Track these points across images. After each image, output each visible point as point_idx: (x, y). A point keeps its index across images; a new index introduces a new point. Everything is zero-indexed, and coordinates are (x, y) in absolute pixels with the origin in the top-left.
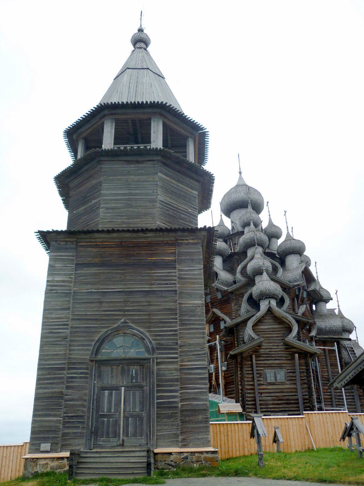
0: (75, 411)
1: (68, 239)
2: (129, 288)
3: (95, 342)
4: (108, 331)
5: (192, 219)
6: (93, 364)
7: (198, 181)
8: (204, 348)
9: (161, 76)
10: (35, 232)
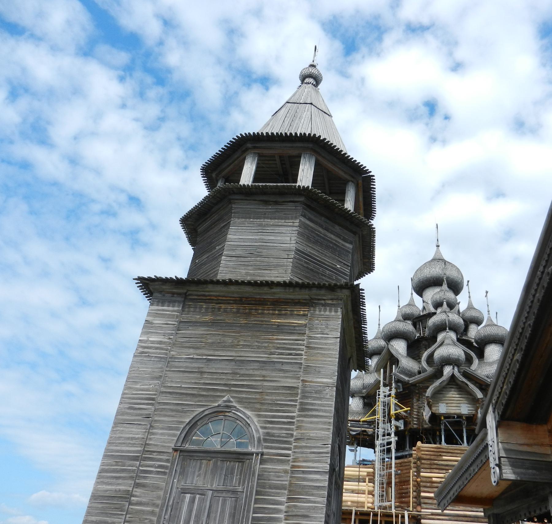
0: (141, 519)
1: (175, 291)
2: (240, 356)
3: (185, 424)
4: (204, 411)
5: (340, 278)
6: (177, 454)
7: (355, 233)
8: (327, 444)
9: (327, 114)
10: (134, 279)
